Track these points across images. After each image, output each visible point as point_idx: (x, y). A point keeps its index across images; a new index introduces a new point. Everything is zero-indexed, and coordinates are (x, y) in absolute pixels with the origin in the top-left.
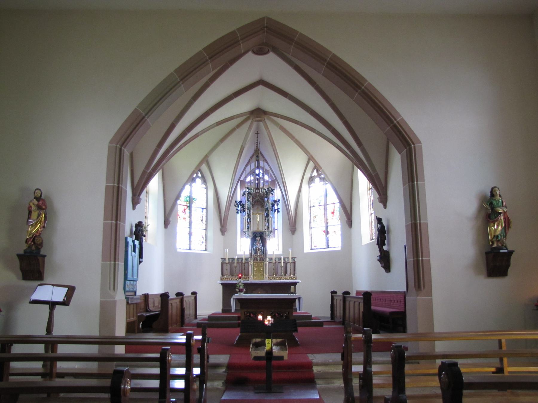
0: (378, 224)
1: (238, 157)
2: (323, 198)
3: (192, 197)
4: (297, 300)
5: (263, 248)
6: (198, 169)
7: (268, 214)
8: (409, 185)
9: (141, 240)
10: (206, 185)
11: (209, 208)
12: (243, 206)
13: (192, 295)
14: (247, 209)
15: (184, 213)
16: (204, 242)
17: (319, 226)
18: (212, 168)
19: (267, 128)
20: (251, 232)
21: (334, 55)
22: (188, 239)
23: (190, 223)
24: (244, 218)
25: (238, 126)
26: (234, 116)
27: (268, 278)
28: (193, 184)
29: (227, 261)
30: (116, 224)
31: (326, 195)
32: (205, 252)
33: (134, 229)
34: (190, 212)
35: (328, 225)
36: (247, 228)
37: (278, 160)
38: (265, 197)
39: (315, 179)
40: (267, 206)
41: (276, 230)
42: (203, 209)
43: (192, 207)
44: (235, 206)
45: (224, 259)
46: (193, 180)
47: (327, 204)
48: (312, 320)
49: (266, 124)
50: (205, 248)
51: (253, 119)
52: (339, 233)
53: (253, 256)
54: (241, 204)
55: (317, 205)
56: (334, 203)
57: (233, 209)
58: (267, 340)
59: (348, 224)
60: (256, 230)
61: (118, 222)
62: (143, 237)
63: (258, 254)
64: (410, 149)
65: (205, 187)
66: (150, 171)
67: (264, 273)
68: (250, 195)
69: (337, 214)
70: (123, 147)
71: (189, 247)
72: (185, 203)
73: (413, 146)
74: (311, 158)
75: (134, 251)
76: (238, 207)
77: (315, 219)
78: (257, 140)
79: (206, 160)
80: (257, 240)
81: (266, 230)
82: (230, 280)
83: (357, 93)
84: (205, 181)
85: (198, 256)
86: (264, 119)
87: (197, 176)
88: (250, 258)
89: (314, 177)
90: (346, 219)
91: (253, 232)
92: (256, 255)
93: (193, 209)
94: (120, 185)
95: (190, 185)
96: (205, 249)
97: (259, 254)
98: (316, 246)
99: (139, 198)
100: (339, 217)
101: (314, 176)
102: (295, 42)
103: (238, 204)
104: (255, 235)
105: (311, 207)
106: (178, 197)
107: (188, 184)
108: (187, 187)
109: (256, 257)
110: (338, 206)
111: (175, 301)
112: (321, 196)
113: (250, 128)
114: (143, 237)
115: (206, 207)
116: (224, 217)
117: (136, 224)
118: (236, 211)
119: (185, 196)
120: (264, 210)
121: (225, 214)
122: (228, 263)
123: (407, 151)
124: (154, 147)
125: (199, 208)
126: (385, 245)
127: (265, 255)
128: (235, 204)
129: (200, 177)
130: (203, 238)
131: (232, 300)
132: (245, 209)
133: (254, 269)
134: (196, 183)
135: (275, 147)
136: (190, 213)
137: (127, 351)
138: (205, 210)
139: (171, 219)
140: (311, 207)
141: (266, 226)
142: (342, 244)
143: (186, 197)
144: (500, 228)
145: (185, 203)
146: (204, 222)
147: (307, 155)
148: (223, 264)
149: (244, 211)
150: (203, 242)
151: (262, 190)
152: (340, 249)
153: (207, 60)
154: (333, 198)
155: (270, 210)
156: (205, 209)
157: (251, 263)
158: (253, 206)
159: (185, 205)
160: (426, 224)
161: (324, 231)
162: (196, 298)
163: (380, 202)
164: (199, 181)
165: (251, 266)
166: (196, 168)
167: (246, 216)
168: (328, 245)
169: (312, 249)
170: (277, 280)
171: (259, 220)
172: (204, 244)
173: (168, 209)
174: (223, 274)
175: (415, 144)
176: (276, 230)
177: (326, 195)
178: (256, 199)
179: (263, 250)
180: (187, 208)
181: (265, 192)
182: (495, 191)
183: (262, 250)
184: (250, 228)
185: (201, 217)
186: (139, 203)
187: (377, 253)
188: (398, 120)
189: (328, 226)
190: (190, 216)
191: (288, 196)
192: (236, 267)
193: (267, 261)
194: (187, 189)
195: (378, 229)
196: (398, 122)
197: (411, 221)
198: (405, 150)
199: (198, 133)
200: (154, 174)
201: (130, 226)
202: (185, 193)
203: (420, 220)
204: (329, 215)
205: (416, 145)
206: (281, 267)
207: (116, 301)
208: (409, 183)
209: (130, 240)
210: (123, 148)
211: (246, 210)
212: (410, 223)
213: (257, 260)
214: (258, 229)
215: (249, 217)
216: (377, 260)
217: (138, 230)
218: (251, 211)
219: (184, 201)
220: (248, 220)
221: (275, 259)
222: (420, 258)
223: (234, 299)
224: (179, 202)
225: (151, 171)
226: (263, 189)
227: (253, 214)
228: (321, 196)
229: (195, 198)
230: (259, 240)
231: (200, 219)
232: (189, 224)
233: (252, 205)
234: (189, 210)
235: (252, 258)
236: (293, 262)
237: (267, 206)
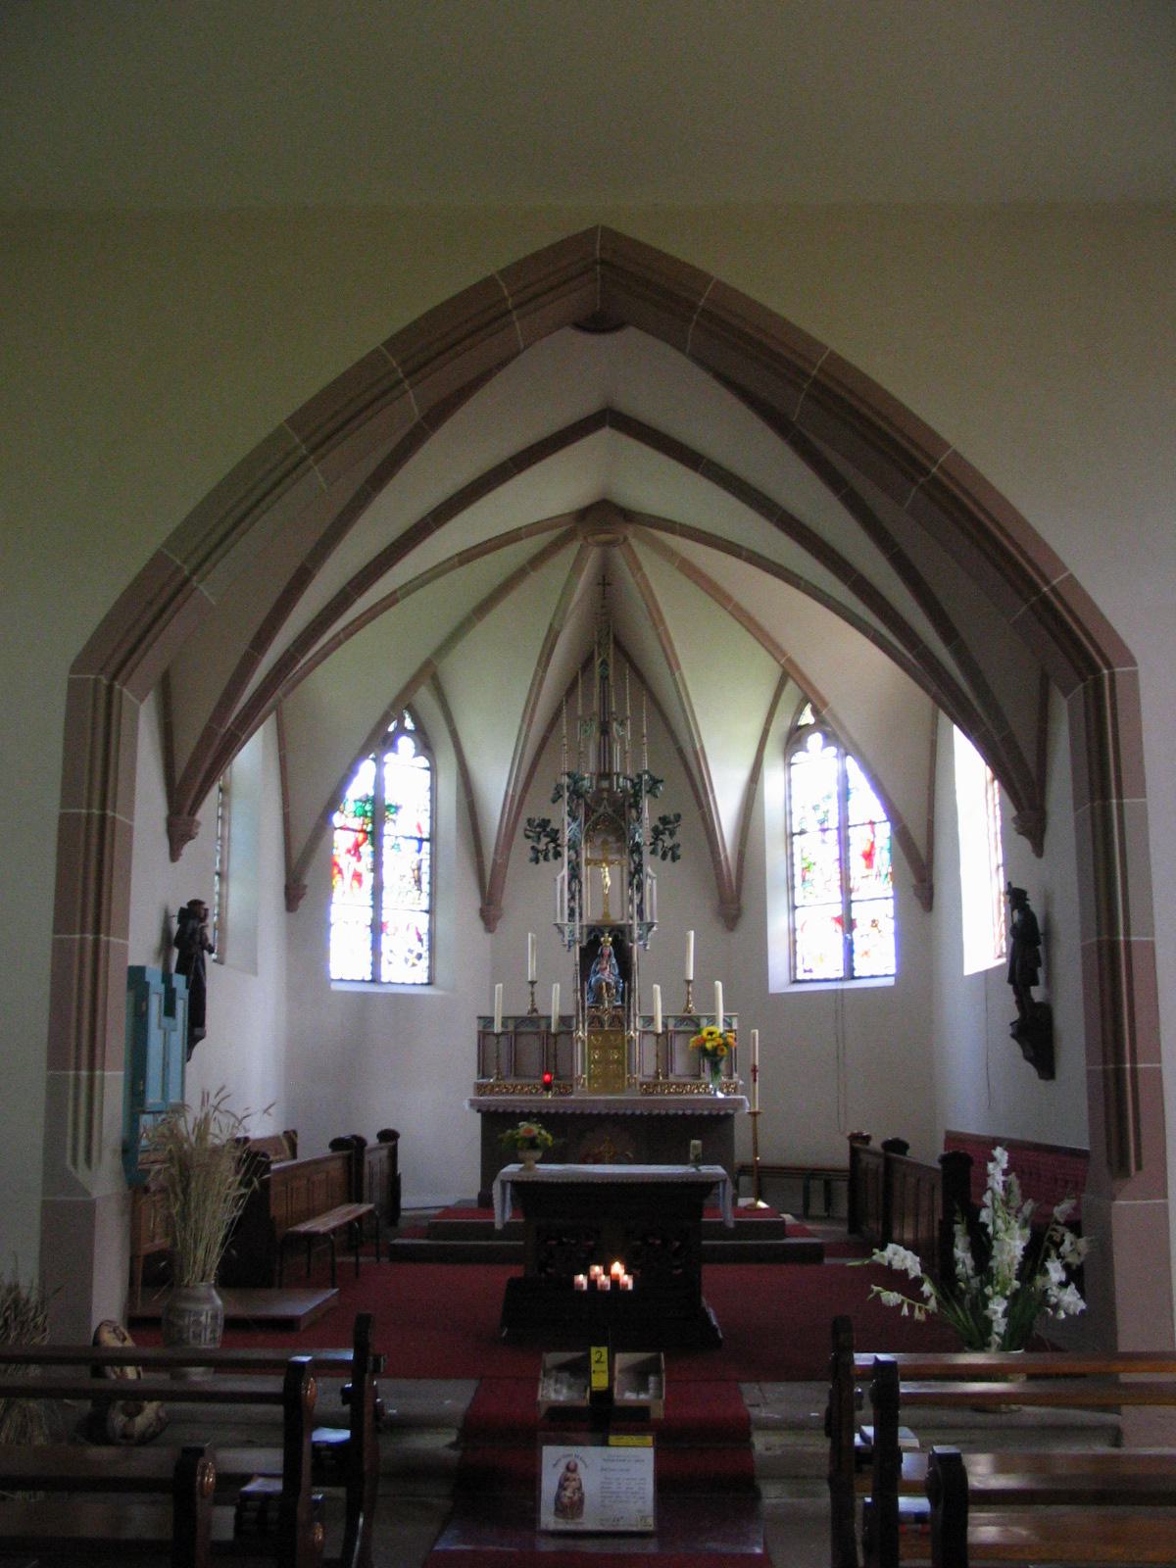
0: (1012, 911)
1: (539, 664)
2: (833, 805)
3: (384, 800)
4: (721, 1184)
6: (403, 702)
7: (640, 865)
8: (1093, 808)
9: (200, 963)
11: (441, 841)
12: (553, 835)
13: (383, 1144)
14: (569, 849)
15: (354, 855)
16: (426, 954)
17: (818, 900)
18: (452, 708)
19: (636, 566)
20: (581, 927)
21: (835, 359)
22: (369, 945)
23: (377, 891)
24: (555, 880)
25: (537, 561)
26: (520, 528)
27: (638, 1088)
28: (389, 757)
29: (497, 1028)
30: (97, 943)
31: (844, 795)
32: (427, 991)
33: (175, 927)
34: (374, 852)
35: (853, 897)
36: (566, 911)
37: (677, 674)
38: (630, 806)
39: (807, 738)
40: (637, 835)
41: (378, 1259)
42: (421, 840)
43: (382, 835)
44: (528, 837)
45: (488, 1021)
46: (388, 743)
47: (850, 824)
48: (785, 1236)
49: (635, 557)
51: (585, 538)
52: (889, 926)
53: (589, 1012)
54: (548, 829)
55: (813, 827)
56: (872, 823)
57: (522, 847)
58: (594, 1350)
59: (920, 897)
60: (600, 918)
61: (102, 936)
62: (206, 953)
63: (603, 1004)
64: (1098, 683)
65: (427, 764)
66: (229, 729)
67: (623, 1069)
68: (578, 798)
69: (883, 859)
70: (116, 683)
71: (372, 974)
72: (356, 823)
73: (1106, 672)
74: (789, 673)
75: (169, 1010)
77: (808, 876)
79: (429, 675)
80: (602, 955)
81: (632, 918)
82: (507, 1093)
83: (914, 490)
84: (426, 746)
85: (401, 1003)
86: (625, 539)
87: (402, 730)
88: (578, 1015)
89: (803, 730)
90: (914, 881)
91: (587, 926)
92: (597, 1008)
93: (387, 842)
94: (110, 813)
95: (374, 760)
96: (429, 978)
97: (606, 1005)
98: (810, 971)
99: (193, 821)
100: (890, 870)
101: (807, 725)
102: (699, 310)
103: (538, 830)
105: (793, 835)
106: (334, 802)
107: (367, 757)
108: (367, 768)
109: (599, 1014)
110: (884, 830)
112: (829, 797)
113: (577, 567)
114: (206, 953)
115: (431, 833)
116: (493, 871)
117: (182, 910)
118: (531, 854)
119: (357, 798)
120: (627, 850)
121: (494, 860)
122: (502, 1033)
123: (1085, 687)
124: (242, 645)
125: (406, 838)
126: (1036, 983)
127: (629, 1008)
128: (526, 830)
129: (410, 731)
130: (420, 940)
132: (559, 845)
133: (589, 1056)
134: (396, 752)
135: (666, 630)
136: (377, 855)
138: (426, 846)
139: (307, 881)
140: (793, 835)
141: (633, 907)
142: (899, 965)
143: (360, 801)
145: (356, 823)
146: (426, 887)
147: (775, 658)
149: (558, 855)
150: (419, 957)
151: (621, 780)
152: (891, 981)
153: (399, 382)
154: (867, 804)
155: (646, 850)
156: (427, 840)
157: (580, 1033)
160: (1150, 947)
161: (839, 920)
163: (1020, 833)
164: (406, 744)
165: (579, 1044)
167: (565, 872)
168: (852, 969)
169: (796, 982)
170: (669, 1093)
171: (609, 884)
172: (425, 963)
174: (483, 1072)
175: (1114, 665)
176: (378, 1259)
177: (844, 795)
178: (601, 810)
179: (624, 988)
180: (365, 839)
181: (629, 785)
183: (620, 989)
184: (577, 914)
185: (414, 871)
186: (192, 838)
187: (1007, 1009)
188: (1054, 582)
189: (852, 902)
190: (377, 867)
191: (714, 798)
193: (635, 1029)
194: (365, 774)
196: (1053, 590)
197: (1099, 934)
198: (1082, 685)
199: (395, 592)
200: (243, 738)
201: (162, 914)
202: (361, 785)
203: (1127, 933)
204: (857, 863)
205: (1117, 670)
207: (95, 1200)
208: (1092, 800)
209: (154, 976)
210: (117, 686)
211: (565, 851)
212: (1094, 939)
213: (602, 1026)
214: (606, 915)
215: (575, 875)
216: (1010, 1038)
217: (189, 931)
218: (583, 852)
219: (355, 816)
220: (569, 883)
221: (663, 1023)
222: (1128, 1066)
223: (503, 1184)
224: (337, 819)
225: (232, 728)
226: (625, 778)
227: (588, 862)
228: (829, 797)
229: (394, 804)
230: (609, 956)
231: (410, 876)
232: (373, 894)
233: (587, 835)
234: (373, 844)
235: (583, 1016)
237: (637, 839)
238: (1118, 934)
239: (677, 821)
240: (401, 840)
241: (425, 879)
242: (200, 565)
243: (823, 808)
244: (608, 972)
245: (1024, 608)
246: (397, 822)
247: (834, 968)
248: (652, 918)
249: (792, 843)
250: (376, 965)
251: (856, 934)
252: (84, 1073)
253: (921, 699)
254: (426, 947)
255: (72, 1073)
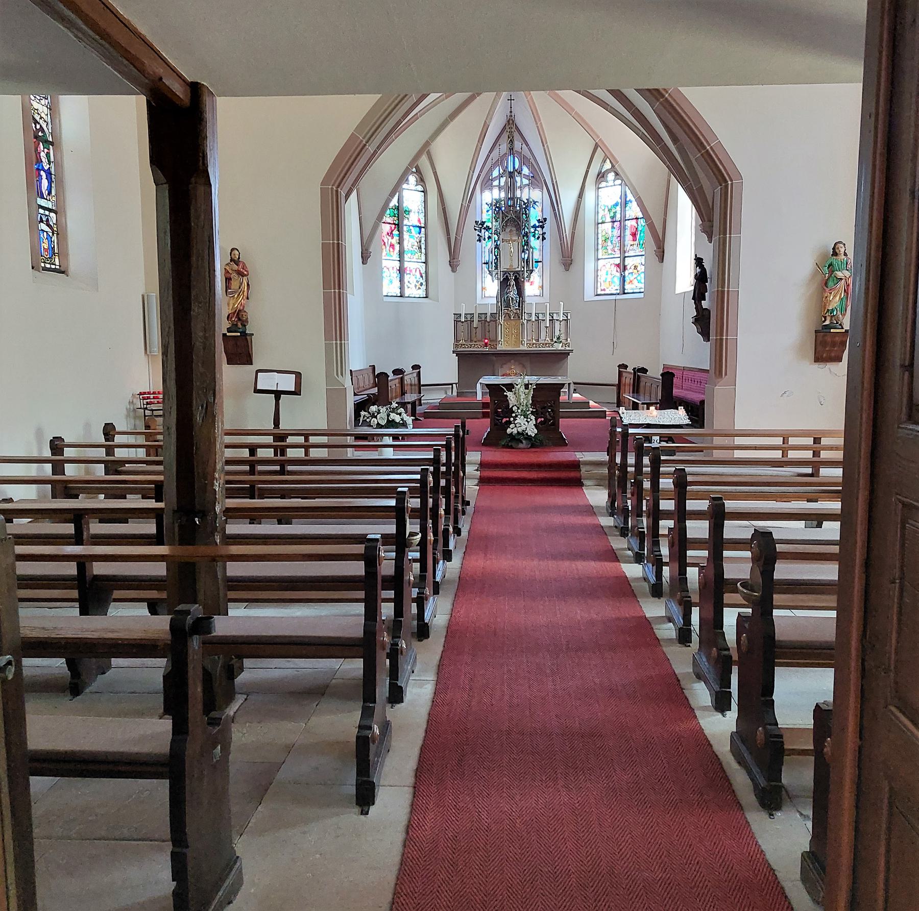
5: (520, 298)
10: (424, 186)
16: (424, 283)
23: (401, 254)
30: (339, 292)
37: (539, 123)
42: (420, 228)
50: (425, 293)
56: (637, 219)
76: (480, 232)
78: (511, 112)
80: (510, 285)
104: (507, 276)
111: (393, 382)
123: (721, 188)
130: (422, 277)
131: (478, 385)
137: (148, 454)
140: (598, 224)
144: (838, 298)
145: (389, 220)
146: (423, 251)
148: (456, 322)
158: (504, 228)
159: (392, 222)
161: (618, 266)
162: (419, 373)
166: (411, 164)
168: (624, 289)
172: (424, 287)
173: (367, 233)
182: (838, 248)
190: (400, 242)
192: (476, 328)
195: (697, 274)
203: (728, 287)
206: (547, 327)
213: (510, 318)
214: (511, 266)
236: (565, 320)
238: (724, 288)
239: (545, 221)
240: (411, 228)
241: (423, 247)
242: (369, 139)
243: (614, 210)
244: (513, 293)
245: (699, 155)
246: (410, 219)
247: (615, 287)
248: (533, 268)
249: (598, 228)
250: (402, 288)
251: (627, 272)
252: (338, 342)
253: (662, 168)
254: (424, 280)
255: (334, 342)
